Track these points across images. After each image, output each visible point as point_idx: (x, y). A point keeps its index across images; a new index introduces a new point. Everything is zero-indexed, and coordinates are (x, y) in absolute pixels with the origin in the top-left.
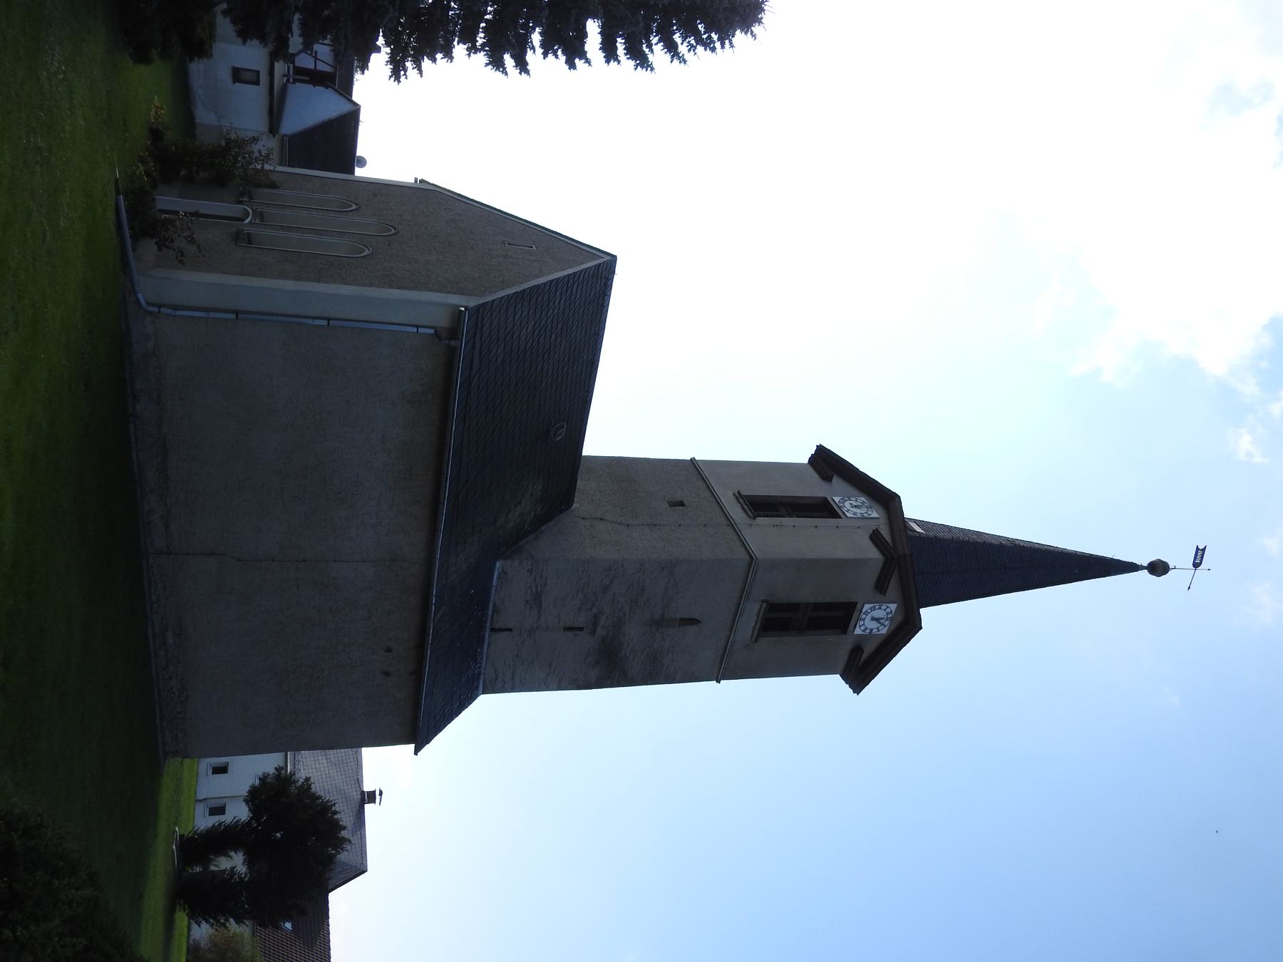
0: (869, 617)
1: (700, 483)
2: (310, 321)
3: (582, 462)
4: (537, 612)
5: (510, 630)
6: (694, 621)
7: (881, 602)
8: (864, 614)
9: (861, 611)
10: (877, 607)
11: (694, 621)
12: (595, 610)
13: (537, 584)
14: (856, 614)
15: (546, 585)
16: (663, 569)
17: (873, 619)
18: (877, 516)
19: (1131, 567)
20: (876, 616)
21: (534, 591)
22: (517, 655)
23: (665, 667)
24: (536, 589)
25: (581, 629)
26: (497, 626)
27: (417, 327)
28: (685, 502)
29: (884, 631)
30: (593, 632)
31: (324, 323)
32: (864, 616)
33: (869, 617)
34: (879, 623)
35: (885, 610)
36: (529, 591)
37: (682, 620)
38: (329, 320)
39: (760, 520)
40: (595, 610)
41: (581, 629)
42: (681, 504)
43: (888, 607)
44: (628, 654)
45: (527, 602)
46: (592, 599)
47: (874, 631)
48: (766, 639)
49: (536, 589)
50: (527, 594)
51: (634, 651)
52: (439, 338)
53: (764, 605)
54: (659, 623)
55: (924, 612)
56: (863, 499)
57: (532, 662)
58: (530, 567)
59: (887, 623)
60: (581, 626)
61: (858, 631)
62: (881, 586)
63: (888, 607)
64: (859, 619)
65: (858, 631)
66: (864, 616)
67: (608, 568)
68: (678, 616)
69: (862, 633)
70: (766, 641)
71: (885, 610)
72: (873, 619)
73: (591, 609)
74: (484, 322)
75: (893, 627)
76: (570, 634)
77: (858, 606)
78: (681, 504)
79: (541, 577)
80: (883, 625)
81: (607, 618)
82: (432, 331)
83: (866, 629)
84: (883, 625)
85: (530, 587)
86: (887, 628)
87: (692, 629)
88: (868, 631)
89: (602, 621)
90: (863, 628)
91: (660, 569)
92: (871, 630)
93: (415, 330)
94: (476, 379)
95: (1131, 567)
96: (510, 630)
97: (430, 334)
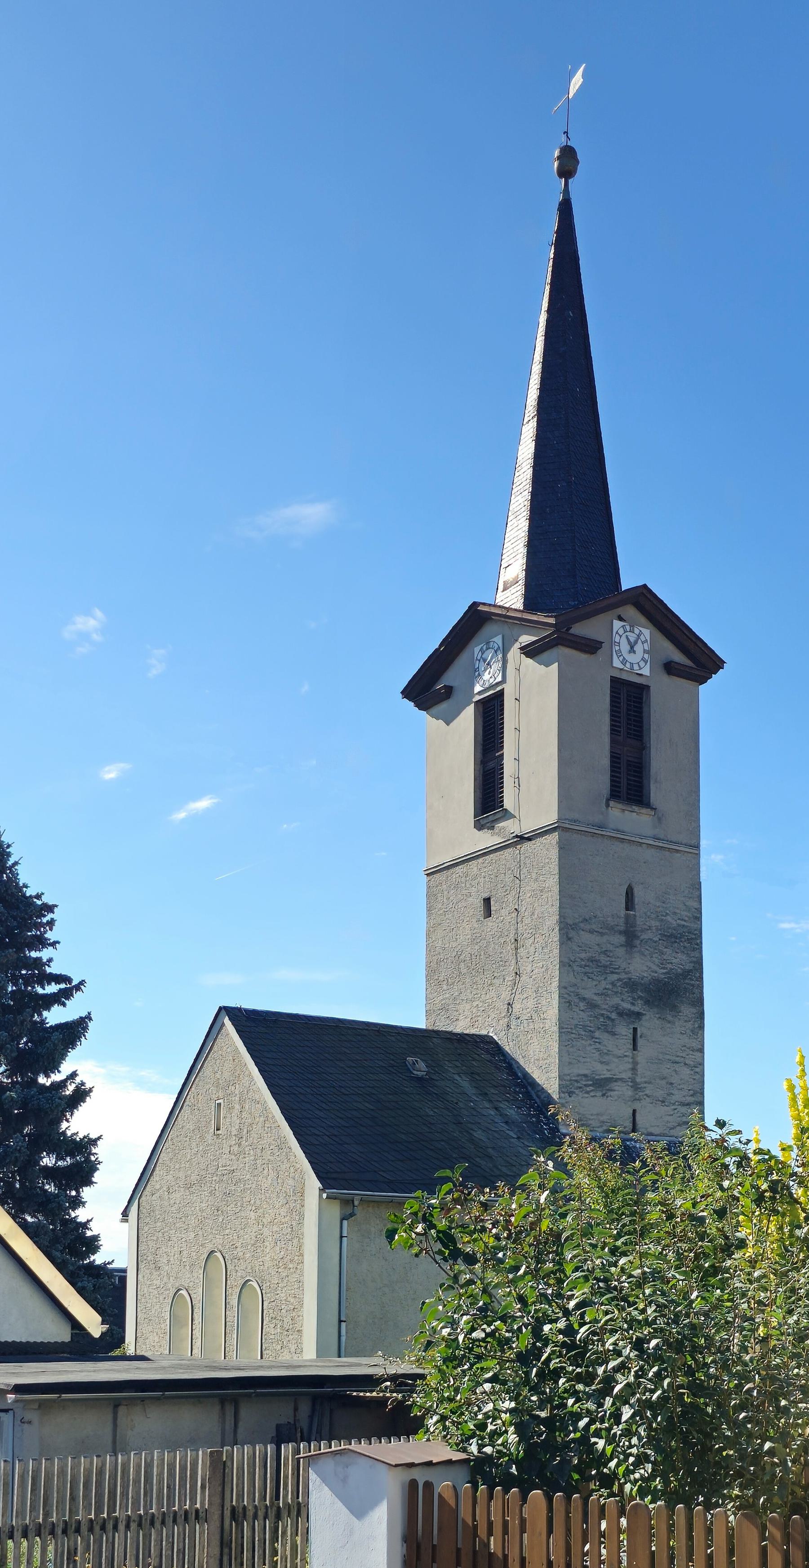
0: (631, 658)
1: (459, 869)
2: (343, 1339)
3: (430, 1028)
4: (615, 1084)
5: (634, 1111)
6: (630, 895)
7: (612, 643)
8: (625, 665)
9: (621, 669)
10: (617, 648)
11: (630, 895)
12: (614, 1016)
13: (585, 1085)
14: (624, 676)
15: (585, 1076)
16: (569, 939)
17: (632, 650)
18: (500, 636)
19: (565, 209)
20: (628, 647)
21: (592, 1088)
22: (663, 1102)
23: (683, 923)
24: (590, 1085)
25: (635, 1030)
26: (629, 1126)
27: (341, 1237)
28: (486, 895)
29: (646, 633)
30: (638, 1015)
31: (343, 1325)
32: (628, 665)
33: (631, 658)
34: (636, 642)
35: (621, 636)
36: (592, 1094)
37: (627, 909)
38: (340, 1321)
39: (508, 802)
40: (614, 1016)
41: (635, 1030)
42: (487, 901)
43: (617, 633)
44: (665, 971)
45: (603, 1095)
46: (602, 1020)
47: (646, 648)
48: (652, 795)
49: (590, 1085)
50: (595, 1096)
51: (662, 964)
52: (352, 1215)
53: (612, 803)
54: (630, 936)
55: (626, 583)
56: (477, 650)
57: (671, 1084)
58: (567, 1094)
59: (637, 631)
60: (631, 1031)
61: (646, 671)
62: (591, 647)
63: (617, 633)
64: (631, 672)
65: (646, 671)
66: (628, 665)
67: (568, 1004)
68: (623, 912)
69: (649, 663)
70: (656, 795)
71: (621, 636)
72: (632, 650)
73: (613, 1020)
74: (339, 1170)
75: (643, 619)
76: (640, 1042)
77: (617, 674)
78: (487, 901)
79: (577, 1081)
80: (639, 636)
81: (622, 1000)
82: (345, 1223)
83: (643, 659)
84: (639, 636)
85: (588, 1092)
86: (643, 630)
87: (638, 892)
88: (646, 656)
89: (627, 1006)
90: (642, 664)
91: (569, 942)
92: (645, 651)
93: (345, 1239)
94: (384, 1175)
95: (565, 209)
96: (634, 1111)
97: (348, 1225)
